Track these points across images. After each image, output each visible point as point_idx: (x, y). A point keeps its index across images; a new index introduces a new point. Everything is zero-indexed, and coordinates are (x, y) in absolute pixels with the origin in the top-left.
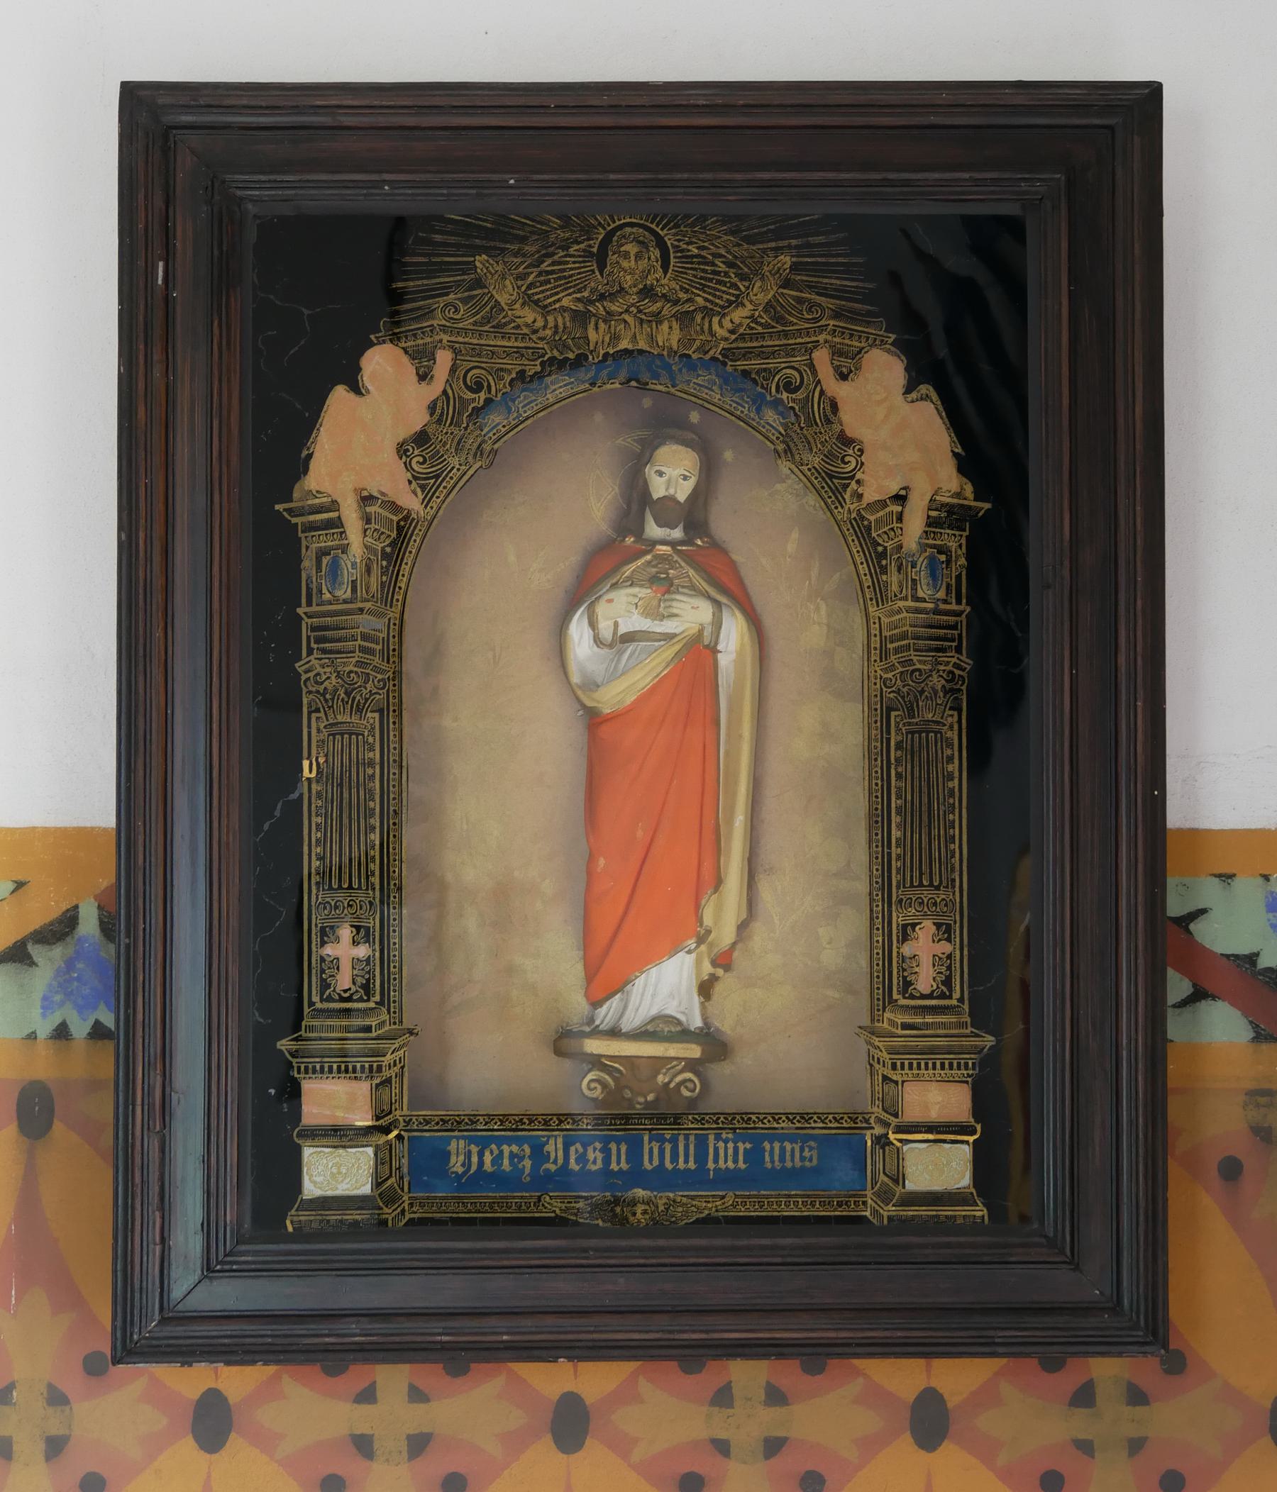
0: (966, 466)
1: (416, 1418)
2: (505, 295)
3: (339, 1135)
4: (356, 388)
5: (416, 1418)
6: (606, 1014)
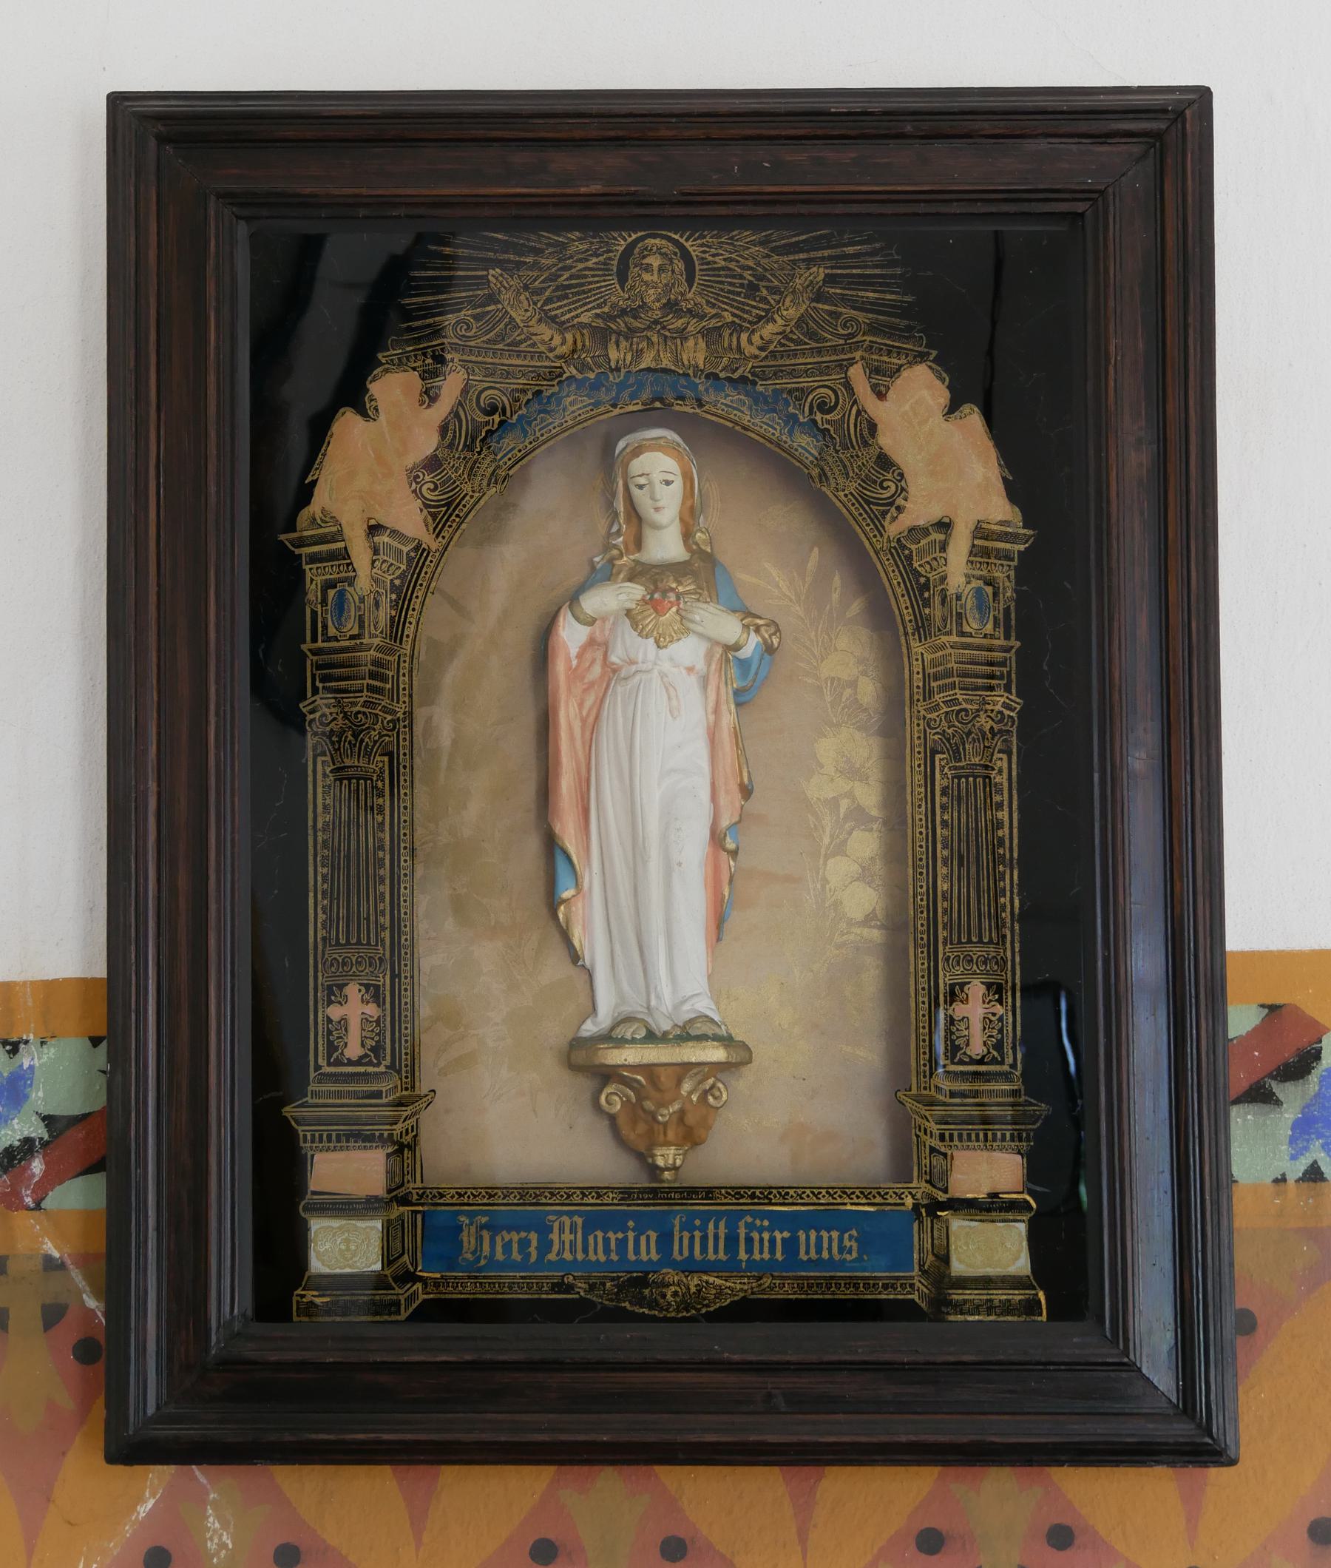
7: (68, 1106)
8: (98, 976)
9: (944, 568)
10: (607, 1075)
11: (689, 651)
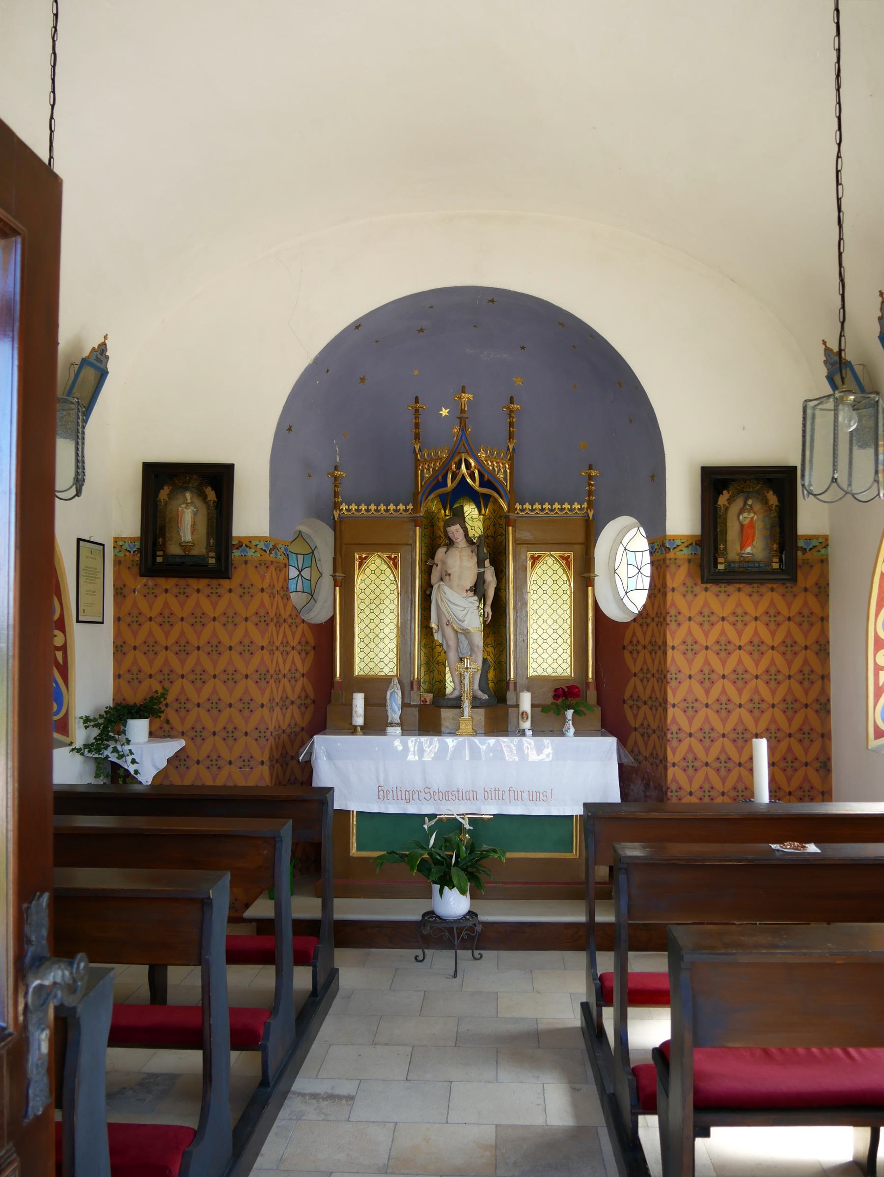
0: (779, 501)
1: (725, 589)
2: (177, 481)
3: (721, 563)
4: (722, 494)
5: (725, 589)
6: (743, 552)
7: (139, 547)
8: (577, 1026)
9: (823, 551)
10: (182, 546)
11: (190, 510)
